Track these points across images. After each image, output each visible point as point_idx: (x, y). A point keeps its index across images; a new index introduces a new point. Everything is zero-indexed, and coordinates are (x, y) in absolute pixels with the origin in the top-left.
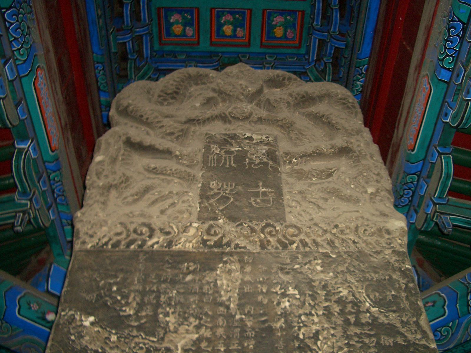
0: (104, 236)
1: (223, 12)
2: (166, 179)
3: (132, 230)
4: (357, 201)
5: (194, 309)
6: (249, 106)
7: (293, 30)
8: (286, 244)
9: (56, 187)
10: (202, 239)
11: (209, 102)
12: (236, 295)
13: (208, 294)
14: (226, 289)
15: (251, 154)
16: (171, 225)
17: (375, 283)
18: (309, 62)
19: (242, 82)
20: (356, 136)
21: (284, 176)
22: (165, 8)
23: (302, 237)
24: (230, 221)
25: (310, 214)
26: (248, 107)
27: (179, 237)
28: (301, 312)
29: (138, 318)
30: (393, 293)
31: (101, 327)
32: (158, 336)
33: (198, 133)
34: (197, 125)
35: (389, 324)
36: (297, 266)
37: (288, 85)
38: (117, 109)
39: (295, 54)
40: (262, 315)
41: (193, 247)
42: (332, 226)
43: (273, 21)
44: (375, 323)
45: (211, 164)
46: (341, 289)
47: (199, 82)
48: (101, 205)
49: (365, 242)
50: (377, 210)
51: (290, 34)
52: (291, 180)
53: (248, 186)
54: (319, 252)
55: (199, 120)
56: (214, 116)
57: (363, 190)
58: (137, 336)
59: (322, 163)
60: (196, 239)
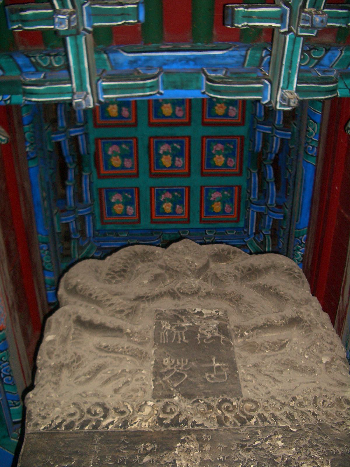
0: (57, 417)
1: (162, 190)
2: (118, 357)
3: (85, 410)
4: (313, 371)
6: (197, 281)
7: (231, 204)
8: (244, 419)
9: (3, 367)
10: (159, 418)
11: (156, 278)
15: (202, 330)
16: (126, 404)
17: (341, 458)
19: (188, 258)
20: (305, 306)
21: (237, 350)
22: (106, 188)
23: (260, 411)
24: (185, 398)
25: (267, 388)
26: (196, 283)
27: (135, 416)
33: (147, 310)
34: (146, 302)
36: (257, 443)
37: (234, 259)
38: (66, 288)
39: (234, 228)
41: (149, 426)
42: (290, 399)
43: (211, 197)
45: (163, 341)
47: (146, 259)
48: (53, 386)
49: (325, 413)
50: (334, 379)
51: (228, 209)
52: (244, 354)
53: (201, 361)
54: (279, 427)
55: (147, 297)
56: (163, 293)
57: (318, 359)
59: (274, 334)
60: (151, 418)
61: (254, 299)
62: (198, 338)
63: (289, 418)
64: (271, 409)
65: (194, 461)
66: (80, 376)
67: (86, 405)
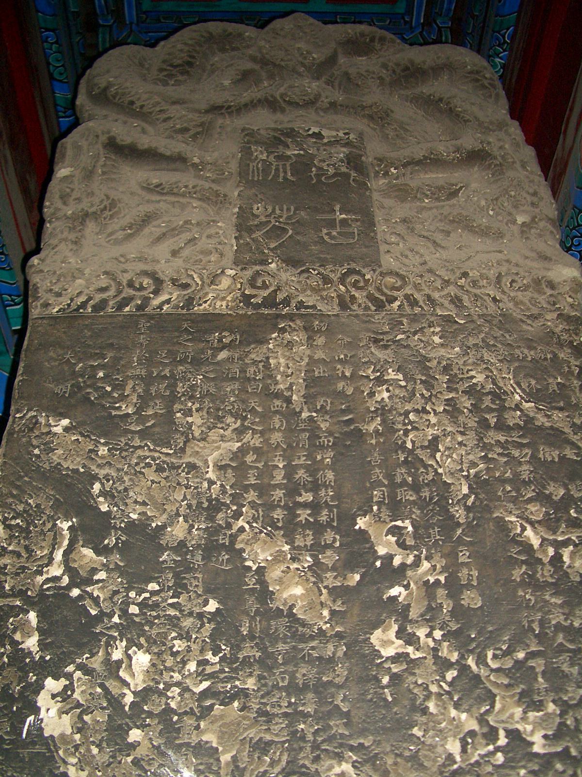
4: (500, 235)
5: (232, 404)
6: (315, 85)
8: (382, 300)
10: (243, 294)
11: (245, 76)
12: (301, 381)
13: (255, 379)
14: (284, 372)
15: (320, 161)
17: (530, 365)
18: (411, 27)
20: (496, 133)
21: (376, 196)
23: (408, 290)
24: (287, 265)
25: (422, 256)
26: (312, 86)
28: (408, 407)
29: (142, 419)
30: (559, 380)
31: (82, 435)
32: (176, 446)
33: (229, 129)
35: (552, 428)
37: (380, 50)
40: (344, 412)
42: (458, 274)
44: (529, 426)
45: (253, 176)
46: (473, 373)
49: (513, 299)
52: (389, 202)
53: (316, 210)
54: (437, 315)
55: (229, 107)
58: (140, 447)
60: (231, 295)
61: (410, 118)
62: (312, 174)
63: (454, 303)
64: (426, 289)
65: (298, 359)
66: (117, 231)
67: (124, 274)
